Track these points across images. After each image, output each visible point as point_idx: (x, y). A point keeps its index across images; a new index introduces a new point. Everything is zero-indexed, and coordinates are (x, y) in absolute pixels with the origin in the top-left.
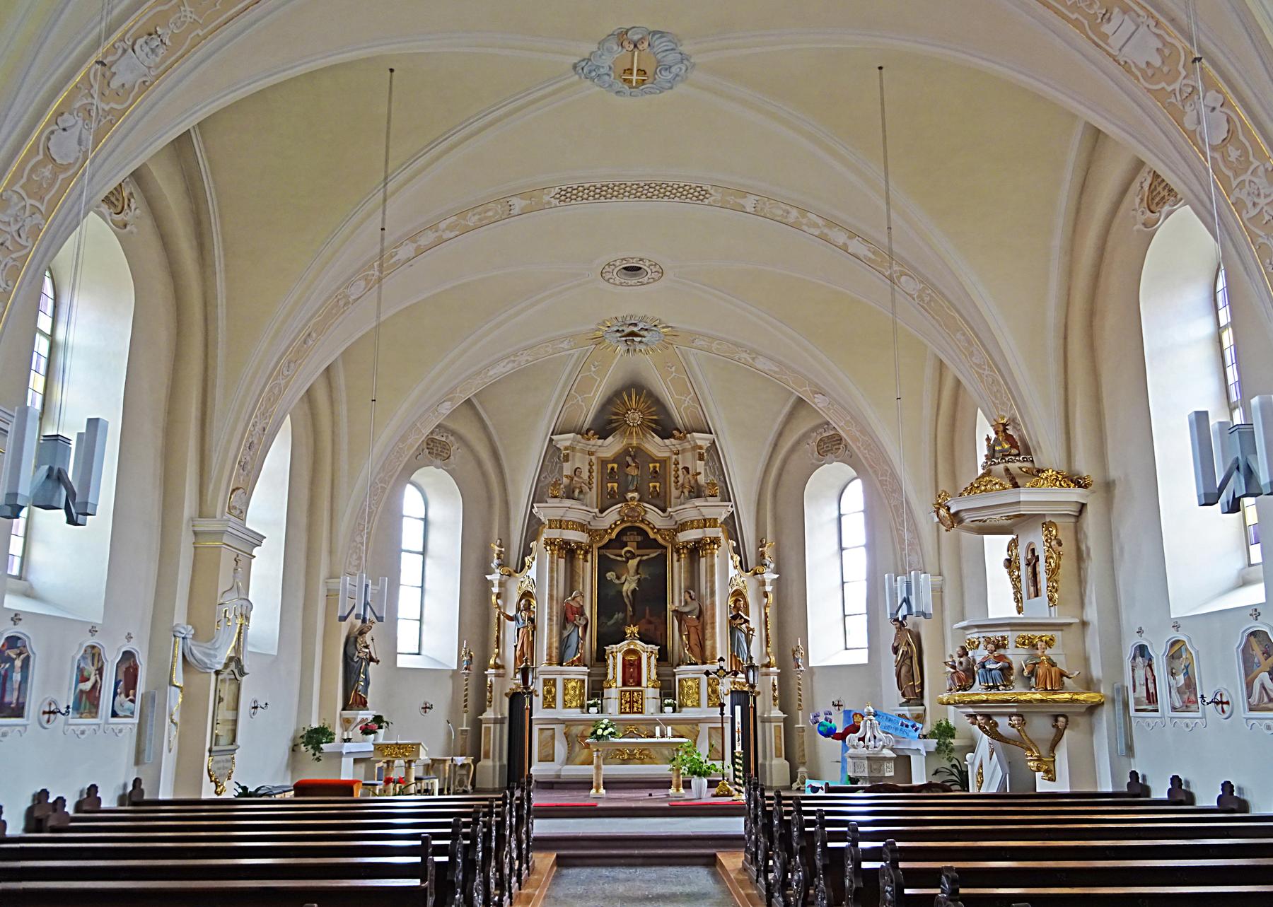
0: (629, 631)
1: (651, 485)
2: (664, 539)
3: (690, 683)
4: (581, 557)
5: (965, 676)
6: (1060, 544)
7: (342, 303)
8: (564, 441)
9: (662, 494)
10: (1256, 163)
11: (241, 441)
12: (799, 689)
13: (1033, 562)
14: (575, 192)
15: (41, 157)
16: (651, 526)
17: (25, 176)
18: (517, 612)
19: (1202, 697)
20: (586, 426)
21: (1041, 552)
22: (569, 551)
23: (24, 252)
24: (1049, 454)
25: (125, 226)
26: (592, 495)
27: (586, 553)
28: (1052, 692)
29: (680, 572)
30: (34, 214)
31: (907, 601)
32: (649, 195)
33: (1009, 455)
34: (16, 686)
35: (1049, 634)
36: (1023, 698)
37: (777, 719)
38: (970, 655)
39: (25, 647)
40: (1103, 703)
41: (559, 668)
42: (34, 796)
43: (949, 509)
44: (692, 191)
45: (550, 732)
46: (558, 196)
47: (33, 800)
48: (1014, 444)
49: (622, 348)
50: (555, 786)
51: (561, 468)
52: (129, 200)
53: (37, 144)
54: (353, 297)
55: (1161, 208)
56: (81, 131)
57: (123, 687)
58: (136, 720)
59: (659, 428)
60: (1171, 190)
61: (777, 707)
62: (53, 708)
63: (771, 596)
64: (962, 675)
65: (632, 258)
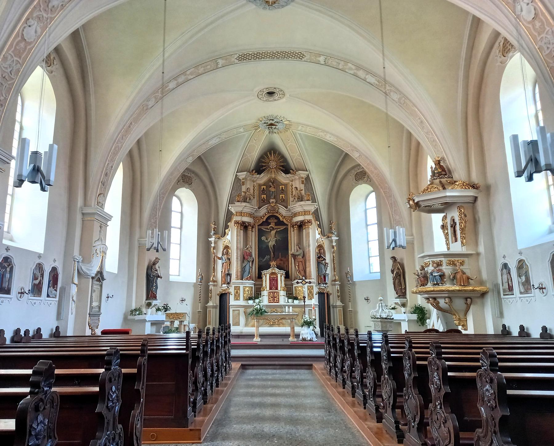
0: (272, 264)
1: (281, 196)
2: (287, 221)
3: (299, 288)
4: (250, 229)
5: (424, 279)
6: (465, 216)
7: (145, 108)
8: (242, 175)
9: (286, 200)
10: (548, 29)
11: (102, 172)
12: (350, 297)
13: (454, 226)
14: (245, 56)
15: (20, 38)
16: (281, 215)
17: (14, 46)
18: (222, 255)
19: (533, 285)
20: (251, 169)
21: (457, 220)
22: (245, 227)
23: (13, 81)
24: (459, 174)
25: (52, 72)
26: (255, 201)
27: (253, 227)
28: (464, 286)
29: (294, 237)
30: (17, 64)
31: (394, 240)
32: (278, 57)
33: (441, 175)
34: (7, 280)
35: (462, 259)
36: (450, 289)
37: (340, 306)
38: (426, 270)
39: (11, 262)
40: (488, 292)
41: (241, 281)
42: (14, 331)
43: (414, 201)
44: (297, 54)
45: (237, 312)
46: (238, 58)
47: (14, 333)
48: (443, 170)
49: (267, 131)
50: (240, 337)
51: (241, 189)
52: (53, 61)
53: (18, 33)
54: (150, 106)
55: (508, 54)
56: (36, 27)
57: (52, 283)
58: (57, 299)
59: (284, 169)
60: (512, 46)
61: (340, 301)
62: (23, 291)
63: (335, 248)
64: (422, 279)
65: (271, 88)
